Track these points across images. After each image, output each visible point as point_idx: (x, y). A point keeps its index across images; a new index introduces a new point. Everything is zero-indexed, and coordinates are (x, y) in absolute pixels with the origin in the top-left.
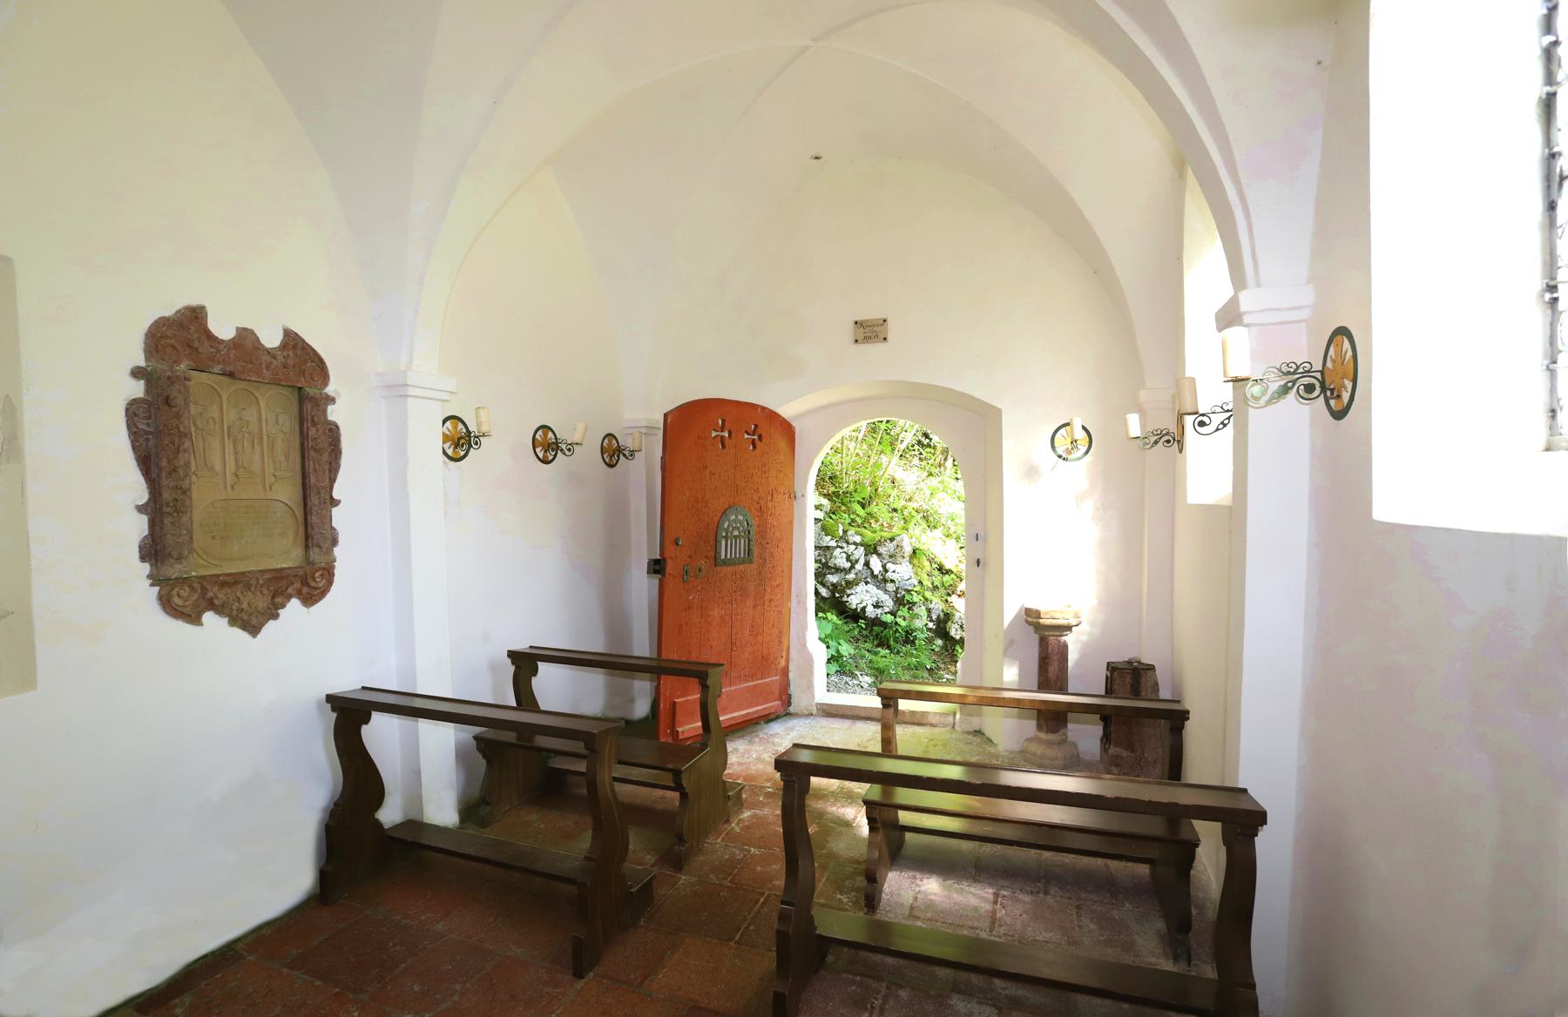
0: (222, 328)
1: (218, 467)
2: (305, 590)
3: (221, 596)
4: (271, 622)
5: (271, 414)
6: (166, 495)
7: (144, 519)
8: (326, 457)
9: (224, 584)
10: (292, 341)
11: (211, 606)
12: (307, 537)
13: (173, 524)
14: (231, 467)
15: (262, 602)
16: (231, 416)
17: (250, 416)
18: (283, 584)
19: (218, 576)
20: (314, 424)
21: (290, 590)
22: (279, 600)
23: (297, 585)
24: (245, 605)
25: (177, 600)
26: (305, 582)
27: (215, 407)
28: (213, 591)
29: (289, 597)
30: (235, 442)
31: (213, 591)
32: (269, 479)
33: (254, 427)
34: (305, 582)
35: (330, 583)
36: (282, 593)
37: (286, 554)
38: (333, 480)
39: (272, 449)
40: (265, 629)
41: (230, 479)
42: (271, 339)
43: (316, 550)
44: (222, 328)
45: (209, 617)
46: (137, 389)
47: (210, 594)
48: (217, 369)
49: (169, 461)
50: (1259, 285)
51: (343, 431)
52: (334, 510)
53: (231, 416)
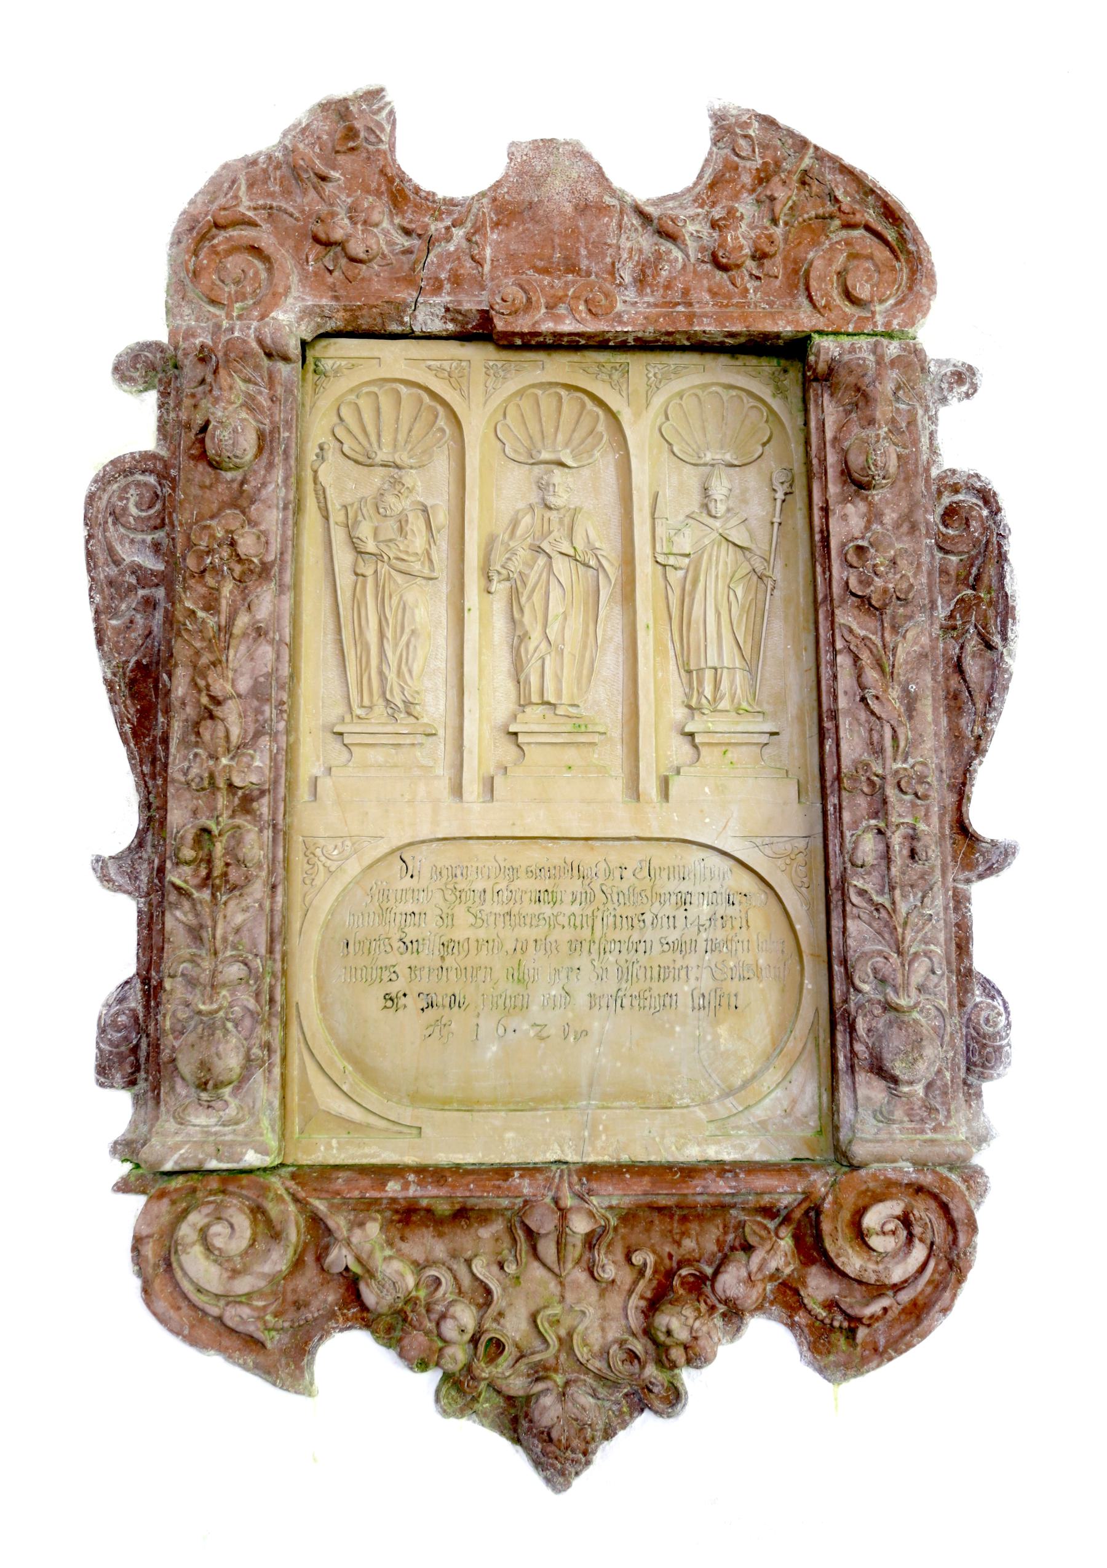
0: (449, 156)
1: (435, 706)
2: (818, 1287)
3: (395, 1270)
4: (646, 1423)
5: (685, 462)
6: (178, 816)
7: (123, 912)
8: (919, 636)
9: (407, 1217)
10: (759, 159)
11: (353, 1302)
12: (838, 1019)
13: (196, 933)
14: (491, 697)
15: (599, 1318)
16: (501, 494)
17: (585, 490)
18: (701, 1242)
19: (382, 1173)
20: (858, 483)
21: (731, 1281)
22: (676, 1322)
23: (779, 1254)
24: (514, 1328)
25: (197, 1266)
26: (812, 1249)
27: (442, 466)
28: (364, 1241)
29: (734, 1314)
30: (514, 596)
31: (364, 1241)
32: (660, 748)
33: (598, 532)
34: (812, 1249)
35: (951, 1266)
36: (699, 1285)
37: (725, 1096)
38: (967, 749)
39: (681, 619)
40: (612, 1457)
41: (482, 746)
42: (657, 161)
43: (871, 1089)
44: (449, 156)
45: (350, 1356)
46: (135, 424)
47: (340, 1257)
48: (428, 316)
49: (198, 671)
50: (341, 1273)
51: (1014, 514)
52: (985, 896)
53: (501, 494)
